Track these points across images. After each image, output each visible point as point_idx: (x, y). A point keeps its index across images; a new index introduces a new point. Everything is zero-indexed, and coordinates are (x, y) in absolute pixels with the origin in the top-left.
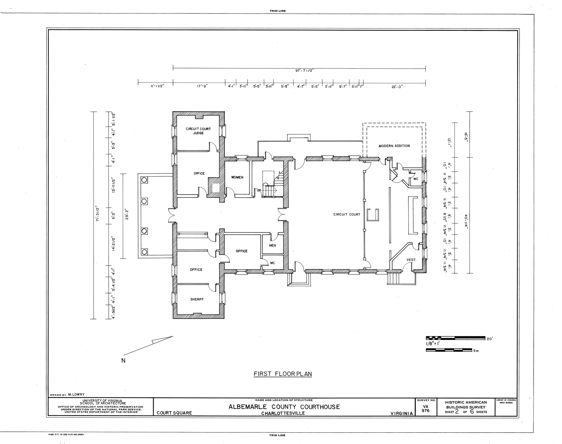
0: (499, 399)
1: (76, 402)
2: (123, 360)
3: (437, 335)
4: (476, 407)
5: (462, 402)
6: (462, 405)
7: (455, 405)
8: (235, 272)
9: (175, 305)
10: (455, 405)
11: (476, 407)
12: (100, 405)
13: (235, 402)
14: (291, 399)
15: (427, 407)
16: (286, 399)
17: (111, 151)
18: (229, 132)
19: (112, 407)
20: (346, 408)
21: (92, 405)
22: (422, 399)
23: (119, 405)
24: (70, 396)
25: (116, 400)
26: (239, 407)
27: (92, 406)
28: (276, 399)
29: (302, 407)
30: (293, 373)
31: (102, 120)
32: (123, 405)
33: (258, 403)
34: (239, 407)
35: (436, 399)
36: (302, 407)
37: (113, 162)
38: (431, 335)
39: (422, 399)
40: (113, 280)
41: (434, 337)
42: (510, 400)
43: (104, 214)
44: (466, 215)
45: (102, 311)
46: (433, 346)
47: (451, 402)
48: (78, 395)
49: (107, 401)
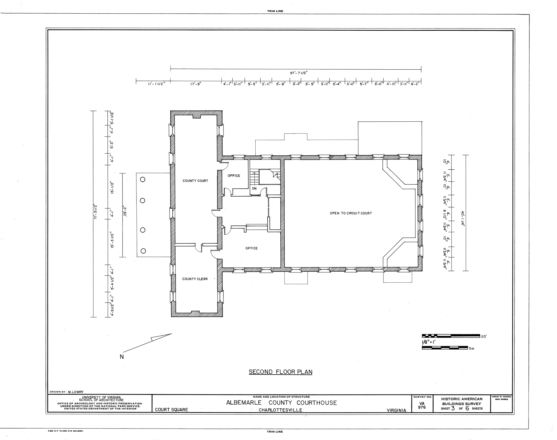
0: (495, 395)
1: (75, 399)
2: (122, 357)
3: (433, 333)
4: (472, 404)
5: (458, 399)
6: (457, 401)
7: (451, 402)
8: (233, 270)
9: (173, 303)
10: (451, 402)
11: (472, 404)
12: (98, 401)
13: (232, 399)
14: (289, 396)
15: (423, 403)
16: (283, 396)
17: (110, 150)
18: (227, 131)
19: (111, 403)
20: (343, 404)
21: (91, 402)
22: (418, 396)
23: (118, 402)
24: (70, 393)
25: (117, 397)
26: (237, 402)
27: (89, 403)
28: (274, 396)
29: (299, 403)
30: (293, 371)
31: (102, 119)
32: (120, 402)
33: (254, 399)
34: (237, 402)
35: (432, 396)
36: (299, 403)
37: (112, 161)
38: (427, 333)
39: (418, 396)
40: (112, 279)
41: (430, 335)
42: (505, 397)
43: (102, 213)
44: (463, 212)
45: (102, 309)
46: (428, 344)
47: (447, 399)
48: (79, 393)
49: (107, 398)
